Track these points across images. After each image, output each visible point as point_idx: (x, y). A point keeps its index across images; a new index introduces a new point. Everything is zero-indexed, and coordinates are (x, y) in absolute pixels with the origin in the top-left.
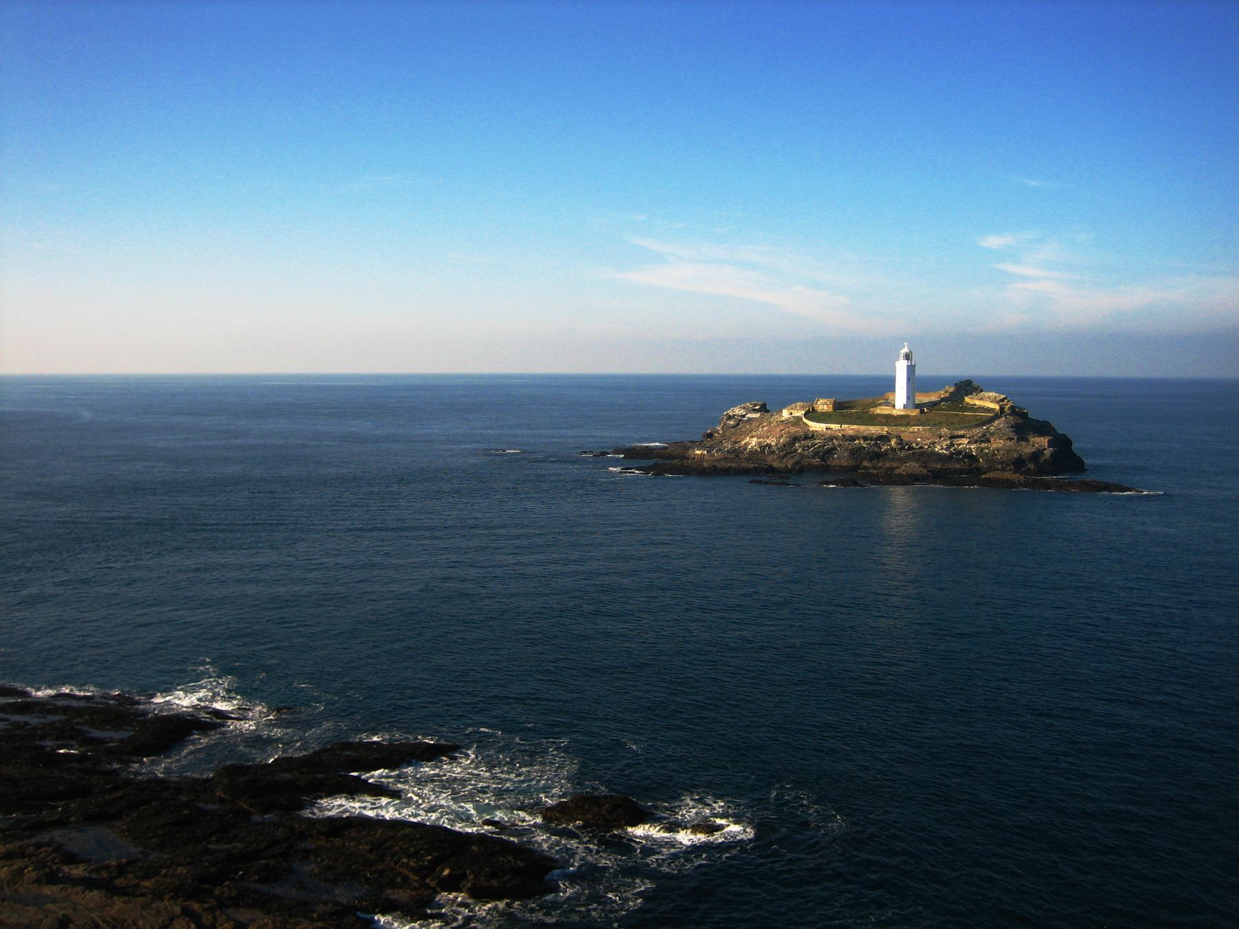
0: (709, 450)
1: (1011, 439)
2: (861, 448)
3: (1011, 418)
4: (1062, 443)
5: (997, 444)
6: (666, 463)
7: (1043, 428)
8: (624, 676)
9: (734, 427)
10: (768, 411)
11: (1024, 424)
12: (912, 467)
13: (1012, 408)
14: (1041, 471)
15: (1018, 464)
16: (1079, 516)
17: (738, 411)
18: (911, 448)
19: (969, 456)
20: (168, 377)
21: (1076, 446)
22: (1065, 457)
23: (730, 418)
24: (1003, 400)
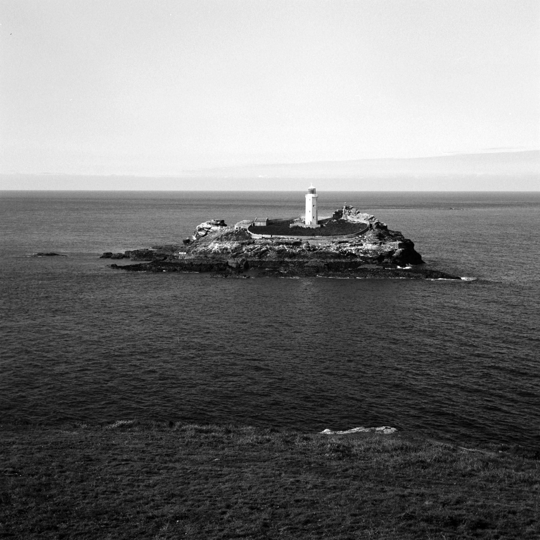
0: (188, 252)
1: (375, 243)
2: (284, 250)
3: (376, 230)
4: (407, 245)
5: (368, 246)
6: (157, 262)
7: (396, 236)
8: (522, 414)
9: (203, 236)
10: (226, 225)
11: (383, 233)
12: (313, 262)
13: (377, 223)
14: (395, 262)
15: (380, 258)
16: (416, 298)
17: (205, 225)
18: (314, 250)
19: (351, 254)
20: (192, 193)
21: (416, 248)
22: (409, 254)
23: (201, 230)
24: (372, 218)
